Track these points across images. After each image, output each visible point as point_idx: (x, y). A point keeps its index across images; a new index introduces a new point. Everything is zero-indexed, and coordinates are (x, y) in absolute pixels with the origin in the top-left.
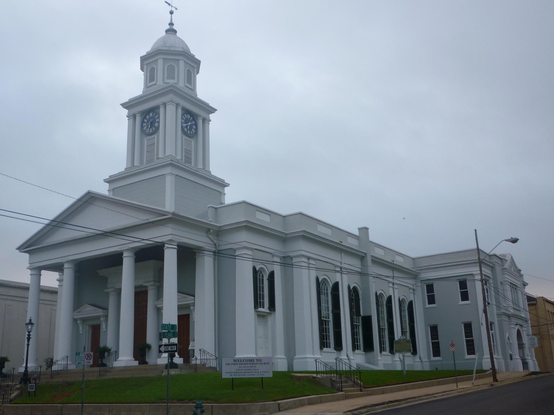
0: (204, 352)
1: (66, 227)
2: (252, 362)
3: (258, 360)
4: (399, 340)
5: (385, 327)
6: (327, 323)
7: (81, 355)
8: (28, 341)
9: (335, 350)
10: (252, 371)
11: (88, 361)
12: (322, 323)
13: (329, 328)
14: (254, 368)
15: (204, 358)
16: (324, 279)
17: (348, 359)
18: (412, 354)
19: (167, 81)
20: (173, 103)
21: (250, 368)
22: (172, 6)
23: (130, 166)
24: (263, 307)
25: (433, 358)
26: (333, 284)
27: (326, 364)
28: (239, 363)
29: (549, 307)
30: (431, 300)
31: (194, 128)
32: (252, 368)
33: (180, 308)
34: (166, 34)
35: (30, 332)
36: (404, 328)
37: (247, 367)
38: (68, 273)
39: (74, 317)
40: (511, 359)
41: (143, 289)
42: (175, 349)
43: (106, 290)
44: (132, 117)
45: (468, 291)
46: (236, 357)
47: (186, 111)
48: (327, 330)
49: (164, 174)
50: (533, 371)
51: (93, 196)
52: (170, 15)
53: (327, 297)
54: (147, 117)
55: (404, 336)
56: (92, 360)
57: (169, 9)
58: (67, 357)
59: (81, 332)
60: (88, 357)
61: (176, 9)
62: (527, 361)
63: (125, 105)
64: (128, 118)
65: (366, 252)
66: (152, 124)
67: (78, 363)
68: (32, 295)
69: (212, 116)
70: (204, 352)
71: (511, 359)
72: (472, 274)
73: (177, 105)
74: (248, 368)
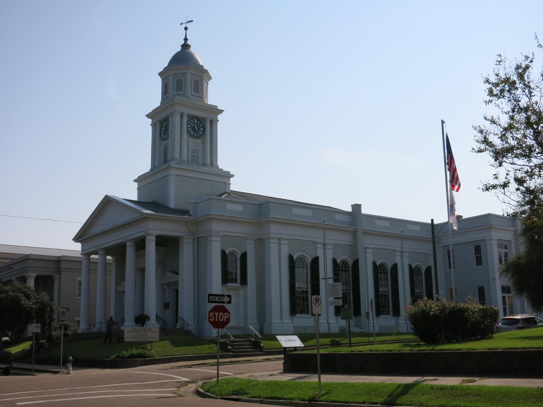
19: (193, 93)
21: (143, 335)
26: (312, 259)
39: (161, 283)
44: (154, 125)
47: (191, 118)
49: (166, 176)
53: (307, 271)
56: (39, 329)
58: (101, 322)
59: (167, 296)
63: (148, 116)
64: (151, 127)
65: (356, 227)
67: (31, 331)
69: (219, 117)
72: (484, 240)
74: (142, 335)
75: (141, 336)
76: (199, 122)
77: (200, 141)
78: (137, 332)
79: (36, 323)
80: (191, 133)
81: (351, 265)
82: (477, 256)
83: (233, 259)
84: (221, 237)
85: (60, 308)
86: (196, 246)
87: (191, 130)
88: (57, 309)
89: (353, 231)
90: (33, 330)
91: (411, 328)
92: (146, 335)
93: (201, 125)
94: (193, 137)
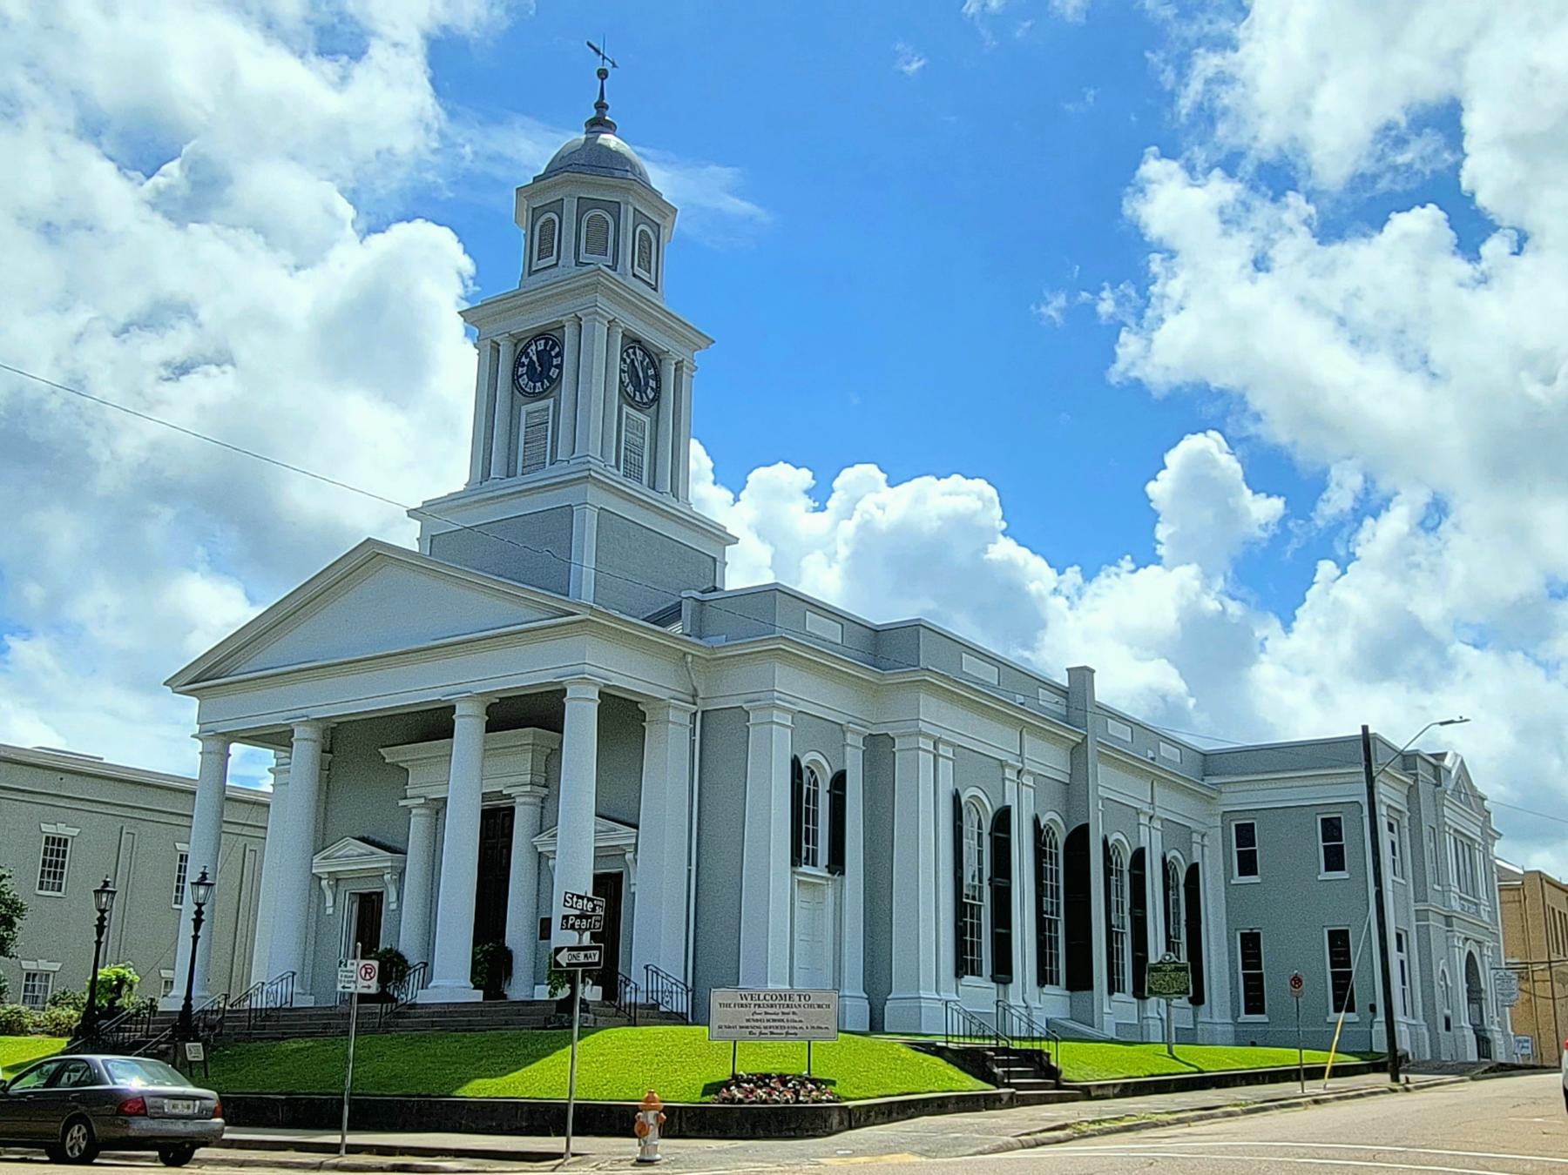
0: (658, 974)
2: (788, 1002)
3: (802, 998)
4: (1160, 962)
5: (1123, 928)
6: (975, 911)
7: (349, 968)
8: (197, 928)
9: (993, 981)
10: (786, 1024)
11: (366, 983)
12: (962, 910)
13: (980, 926)
14: (791, 1017)
15: (633, 1001)
16: (1117, 840)
17: (1027, 1007)
18: (1191, 1000)
19: (637, 270)
22: (604, 58)
24: (815, 864)
25: (1244, 1017)
27: (970, 1017)
28: (753, 1002)
29: (1555, 899)
30: (1248, 864)
31: (652, 388)
32: (785, 1017)
33: (600, 855)
35: (204, 904)
36: (1172, 933)
37: (774, 1014)
38: (305, 749)
40: (1448, 1028)
41: (503, 803)
42: (597, 960)
43: (402, 803)
45: (1342, 846)
46: (460, 1092)
47: (633, 342)
48: (976, 930)
50: (1504, 1061)
51: (379, 554)
55: (1172, 954)
56: (376, 978)
60: (366, 972)
61: (614, 65)
62: (1489, 1035)
68: (203, 809)
70: (658, 974)
71: (1448, 1028)
74: (774, 1017)
75: (774, 1020)
76: (647, 360)
78: (759, 1006)
79: (363, 958)
80: (628, 389)
81: (1064, 840)
84: (794, 714)
85: (575, 899)
86: (698, 738)
87: (627, 381)
88: (565, 900)
90: (352, 985)
92: (796, 1018)
93: (651, 372)
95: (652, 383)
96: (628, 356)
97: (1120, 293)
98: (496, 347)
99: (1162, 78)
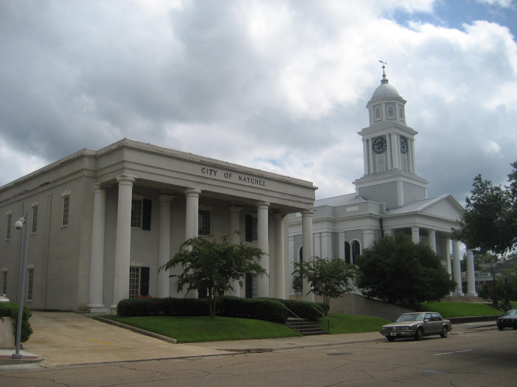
1: (191, 195)
19: (389, 118)
20: (395, 134)
23: (367, 173)
34: (381, 84)
47: (402, 137)
52: (383, 69)
54: (376, 141)
57: (382, 65)
61: (386, 64)
66: (382, 146)
69: (415, 137)
73: (397, 134)
77: (384, 154)
82: (135, 275)
83: (135, 279)
89: (379, 218)
91: (336, 289)
94: (379, 153)
95: (406, 146)
96: (402, 140)
97: (482, 259)
98: (368, 141)
99: (489, 251)
